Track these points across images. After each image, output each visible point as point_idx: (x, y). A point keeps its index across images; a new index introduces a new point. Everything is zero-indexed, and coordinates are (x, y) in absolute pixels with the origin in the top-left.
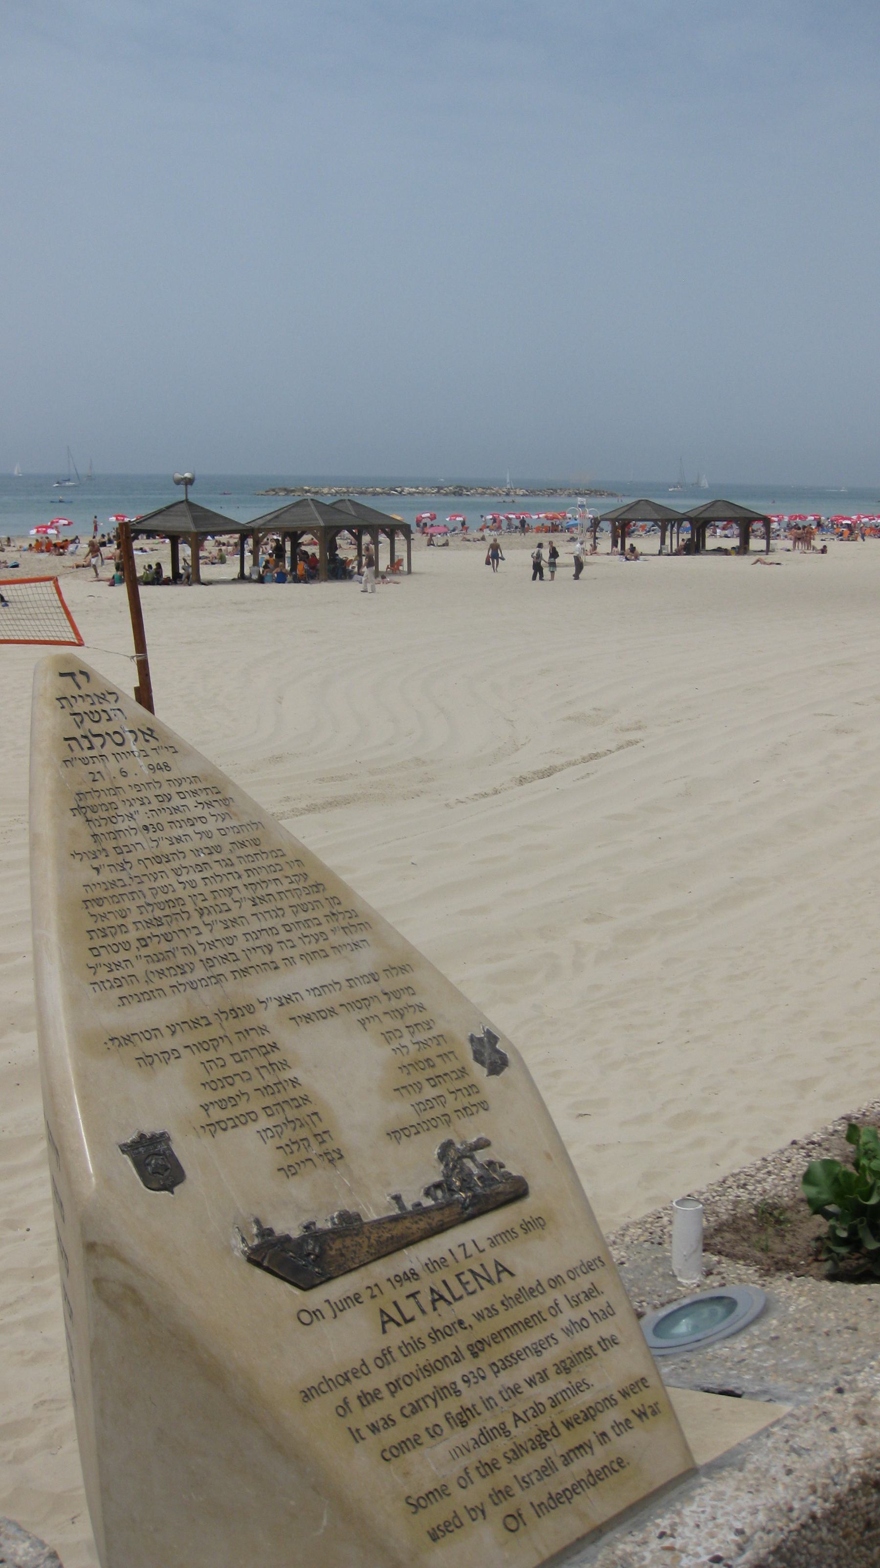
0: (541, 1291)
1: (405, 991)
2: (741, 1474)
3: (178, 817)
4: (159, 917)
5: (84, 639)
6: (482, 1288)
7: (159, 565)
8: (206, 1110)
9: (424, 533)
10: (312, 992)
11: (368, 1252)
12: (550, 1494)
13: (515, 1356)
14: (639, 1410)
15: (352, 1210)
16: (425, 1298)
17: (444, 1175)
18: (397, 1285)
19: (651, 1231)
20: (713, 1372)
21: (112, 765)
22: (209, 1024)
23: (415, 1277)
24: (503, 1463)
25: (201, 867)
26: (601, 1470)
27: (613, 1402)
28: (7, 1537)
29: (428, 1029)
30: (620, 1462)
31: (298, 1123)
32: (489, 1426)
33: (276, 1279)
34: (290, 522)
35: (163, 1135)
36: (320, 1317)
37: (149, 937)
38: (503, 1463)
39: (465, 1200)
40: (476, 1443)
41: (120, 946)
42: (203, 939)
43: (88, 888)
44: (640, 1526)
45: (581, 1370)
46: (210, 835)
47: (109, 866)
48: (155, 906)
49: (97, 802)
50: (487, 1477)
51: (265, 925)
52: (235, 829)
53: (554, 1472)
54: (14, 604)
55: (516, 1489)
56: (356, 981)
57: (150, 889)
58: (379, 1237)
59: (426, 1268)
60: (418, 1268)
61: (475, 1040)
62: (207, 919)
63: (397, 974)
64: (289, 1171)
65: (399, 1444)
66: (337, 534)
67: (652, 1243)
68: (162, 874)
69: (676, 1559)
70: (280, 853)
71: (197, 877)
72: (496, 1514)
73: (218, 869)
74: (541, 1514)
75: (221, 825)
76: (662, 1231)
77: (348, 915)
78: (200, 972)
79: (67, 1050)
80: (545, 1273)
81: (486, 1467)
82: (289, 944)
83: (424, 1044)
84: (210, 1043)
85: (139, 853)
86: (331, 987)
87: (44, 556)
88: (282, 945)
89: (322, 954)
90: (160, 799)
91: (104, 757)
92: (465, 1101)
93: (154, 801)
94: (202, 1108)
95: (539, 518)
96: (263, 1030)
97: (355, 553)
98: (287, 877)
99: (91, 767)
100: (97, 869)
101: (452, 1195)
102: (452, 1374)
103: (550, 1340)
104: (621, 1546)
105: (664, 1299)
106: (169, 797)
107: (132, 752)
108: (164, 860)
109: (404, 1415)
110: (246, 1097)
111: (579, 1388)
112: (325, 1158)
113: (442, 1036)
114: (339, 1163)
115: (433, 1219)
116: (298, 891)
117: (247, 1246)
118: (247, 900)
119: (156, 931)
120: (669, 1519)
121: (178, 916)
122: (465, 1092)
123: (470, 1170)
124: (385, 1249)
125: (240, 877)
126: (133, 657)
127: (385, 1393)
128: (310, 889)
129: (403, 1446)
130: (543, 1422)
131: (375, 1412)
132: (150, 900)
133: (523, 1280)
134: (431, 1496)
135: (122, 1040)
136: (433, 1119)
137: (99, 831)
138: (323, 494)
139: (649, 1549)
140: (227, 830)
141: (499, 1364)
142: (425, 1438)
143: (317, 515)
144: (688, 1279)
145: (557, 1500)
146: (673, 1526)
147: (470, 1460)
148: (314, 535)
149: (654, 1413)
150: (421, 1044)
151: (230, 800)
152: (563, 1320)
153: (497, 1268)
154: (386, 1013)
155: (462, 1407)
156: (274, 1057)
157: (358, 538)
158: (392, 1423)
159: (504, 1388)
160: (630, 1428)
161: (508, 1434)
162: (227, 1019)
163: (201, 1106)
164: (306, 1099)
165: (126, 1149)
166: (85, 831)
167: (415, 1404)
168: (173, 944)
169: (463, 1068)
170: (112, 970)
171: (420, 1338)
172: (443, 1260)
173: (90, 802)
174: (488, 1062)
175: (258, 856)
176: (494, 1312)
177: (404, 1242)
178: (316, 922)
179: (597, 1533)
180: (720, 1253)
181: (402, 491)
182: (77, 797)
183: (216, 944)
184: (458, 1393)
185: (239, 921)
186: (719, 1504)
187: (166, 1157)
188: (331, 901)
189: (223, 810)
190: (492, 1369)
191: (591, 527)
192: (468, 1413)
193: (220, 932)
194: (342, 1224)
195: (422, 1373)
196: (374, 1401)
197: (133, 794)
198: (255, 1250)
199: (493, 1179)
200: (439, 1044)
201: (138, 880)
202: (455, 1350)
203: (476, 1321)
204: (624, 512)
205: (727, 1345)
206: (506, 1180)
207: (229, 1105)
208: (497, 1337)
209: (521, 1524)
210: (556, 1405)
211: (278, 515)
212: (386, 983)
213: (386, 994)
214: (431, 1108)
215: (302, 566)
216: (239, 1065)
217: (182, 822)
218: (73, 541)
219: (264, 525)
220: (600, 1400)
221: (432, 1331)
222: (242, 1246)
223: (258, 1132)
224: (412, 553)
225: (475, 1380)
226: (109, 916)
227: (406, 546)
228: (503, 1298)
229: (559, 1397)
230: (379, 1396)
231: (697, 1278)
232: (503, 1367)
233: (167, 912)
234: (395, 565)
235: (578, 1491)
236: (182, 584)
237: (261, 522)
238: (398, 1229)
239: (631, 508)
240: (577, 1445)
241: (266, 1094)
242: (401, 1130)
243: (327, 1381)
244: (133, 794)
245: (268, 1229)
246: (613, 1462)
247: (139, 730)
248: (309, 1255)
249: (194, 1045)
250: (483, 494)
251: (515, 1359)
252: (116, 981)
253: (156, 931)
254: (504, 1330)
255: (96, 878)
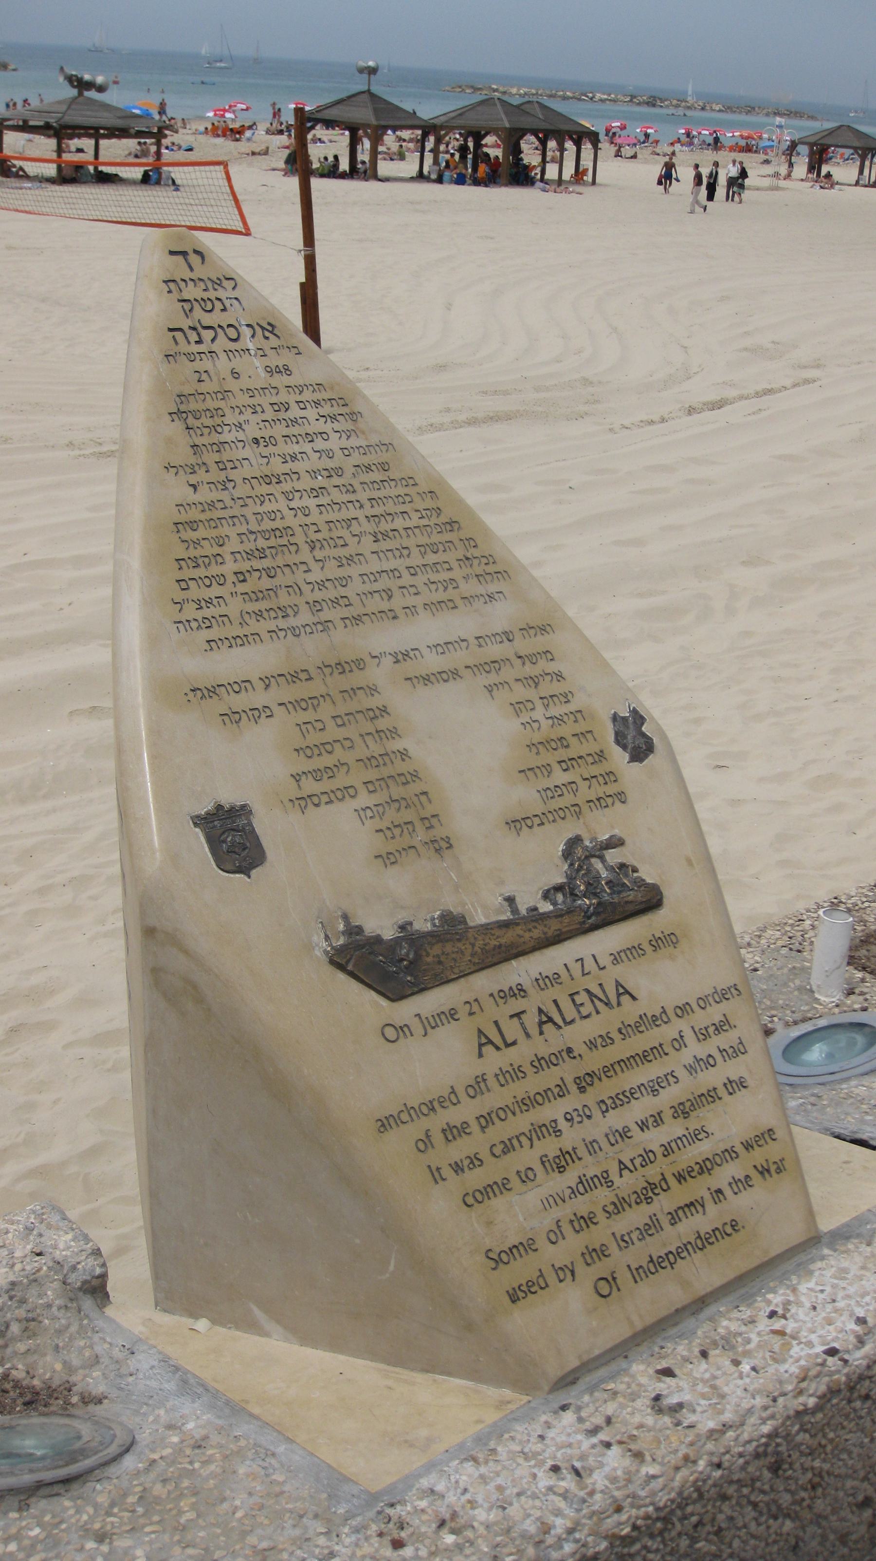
0: (665, 1020)
1: (543, 655)
2: (869, 1249)
3: (295, 430)
4: (263, 548)
5: (252, 230)
6: (598, 1012)
7: (336, 157)
8: (297, 781)
9: (612, 143)
10: (434, 650)
11: (470, 961)
12: (651, 1257)
13: (628, 1094)
14: (762, 1166)
15: (456, 910)
16: (531, 1020)
17: (567, 876)
18: (501, 1001)
19: (791, 935)
20: (847, 1114)
21: (223, 364)
22: (310, 679)
23: (522, 993)
24: (601, 1217)
25: (317, 492)
26: (711, 1233)
27: (734, 1155)
28: (49, 1227)
29: (566, 702)
30: (734, 1224)
31: (403, 803)
32: (590, 1174)
33: (361, 986)
34: (474, 121)
35: (243, 807)
36: (408, 1033)
37: (248, 571)
38: (601, 1217)
39: (589, 908)
40: (573, 1192)
41: (213, 579)
42: (311, 577)
43: (181, 508)
44: (748, 1299)
45: (701, 1115)
46: (331, 455)
47: (208, 483)
48: (258, 534)
49: (201, 406)
50: (581, 1233)
51: (386, 566)
52: (361, 449)
53: (658, 1232)
54: (187, 189)
55: (613, 1248)
56: (487, 639)
57: (254, 514)
58: (485, 945)
59: (535, 983)
60: (527, 984)
61: (618, 719)
62: (319, 554)
63: (535, 635)
64: (388, 859)
65: (485, 1188)
66: (521, 137)
67: (791, 949)
68: (270, 497)
69: (787, 1347)
70: (411, 482)
71: (312, 503)
72: (587, 1275)
73: (338, 496)
74: (638, 1279)
75: (344, 443)
76: (802, 936)
77: (484, 560)
78: (305, 617)
79: (140, 699)
80: (671, 1000)
81: (582, 1221)
82: (413, 590)
83: (560, 720)
84: (309, 702)
85: (246, 471)
86: (456, 645)
87: (220, 141)
88: (405, 591)
89: (451, 605)
90: (302, 405)
91: (214, 355)
92: (599, 790)
93: (269, 410)
94: (292, 779)
95: (733, 136)
96: (373, 690)
97: (539, 159)
98: (417, 511)
99: (198, 365)
100: (194, 487)
101: (574, 901)
102: (554, 1111)
103: (669, 1077)
104: (725, 1323)
105: (798, 1016)
106: (287, 406)
107: (248, 350)
108: (274, 480)
109: (494, 1155)
110: (345, 768)
111: (697, 1135)
112: (431, 846)
113: (580, 711)
114: (447, 853)
115: (549, 928)
116: (428, 529)
117: (330, 945)
118: (332, 560)
119: (257, 564)
120: (783, 1294)
121: (285, 549)
122: (601, 779)
123: (598, 872)
124: (490, 959)
125: (361, 507)
126: (300, 251)
127: (475, 1128)
128: (443, 527)
129: (489, 1191)
130: (652, 1173)
131: (460, 1150)
132: (254, 527)
133: (646, 1006)
134: (515, 1251)
135: (205, 692)
136: (560, 809)
137: (199, 441)
138: (512, 95)
139: (757, 1330)
140: (351, 450)
141: (609, 1102)
142: (515, 1182)
143: (503, 117)
144: (827, 996)
145: (658, 1264)
146: (786, 1304)
147: (564, 1212)
148: (498, 136)
149: (779, 1171)
150: (555, 720)
151: (359, 415)
152: (687, 1056)
153: (617, 990)
154: (517, 680)
155: (561, 1150)
156: (383, 723)
157: (543, 143)
158: (479, 1163)
159: (611, 1131)
160: (750, 1186)
161: (610, 1184)
162: (331, 674)
163: (292, 775)
164: (415, 775)
165: (200, 821)
166: (183, 441)
167: (508, 1143)
168: (276, 581)
169: (601, 751)
170: (201, 608)
171: (520, 1066)
172: (556, 976)
173: (193, 406)
174: (630, 746)
175: (385, 483)
176: (609, 1041)
177: (514, 951)
178: (446, 566)
179: (700, 1304)
180: (864, 969)
181: (594, 97)
182: (177, 399)
183: (327, 584)
184: (558, 1133)
185: (356, 559)
186: (843, 1284)
187: (245, 833)
188: (466, 543)
189: (349, 426)
190: (600, 1108)
191: (787, 150)
192: (567, 1156)
193: (332, 571)
194: (443, 927)
195: (519, 1107)
196: (460, 1135)
197: (244, 399)
198: (340, 951)
199: (624, 885)
200: (576, 721)
201: (241, 502)
202: (561, 1083)
203: (587, 1049)
204: (824, 137)
205: (864, 1083)
206: (639, 887)
207: (325, 776)
208: (609, 1071)
209: (615, 1289)
210: (669, 1154)
211: (462, 113)
212: (522, 645)
213: (520, 657)
214: (559, 796)
215: (483, 168)
216: (342, 729)
217: (299, 437)
218: (250, 127)
219: (446, 122)
220: (719, 1152)
221: (535, 1059)
222: (325, 944)
223: (356, 810)
224: (598, 163)
225: (579, 1119)
226: (203, 543)
227: (592, 156)
228: (621, 1026)
229: (673, 1145)
230: (467, 1131)
231: (837, 997)
232: (613, 1106)
233: (272, 542)
234: (579, 174)
235: (682, 1255)
236: (359, 179)
237: (443, 119)
238: (508, 937)
239: (831, 132)
240: (688, 1203)
241: (369, 766)
242: (523, 819)
243: (409, 1109)
244: (244, 399)
245: (357, 927)
246: (725, 1224)
247: (258, 324)
248: (402, 960)
249: (290, 702)
250: (677, 106)
251: (627, 1097)
252: (205, 621)
253: (257, 564)
254: (618, 1062)
255: (192, 497)
